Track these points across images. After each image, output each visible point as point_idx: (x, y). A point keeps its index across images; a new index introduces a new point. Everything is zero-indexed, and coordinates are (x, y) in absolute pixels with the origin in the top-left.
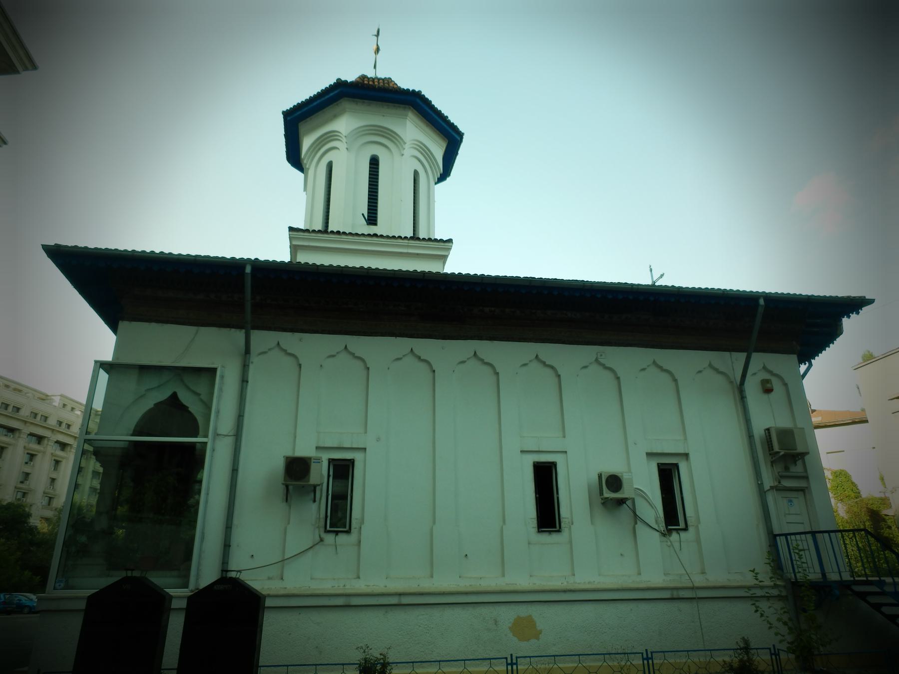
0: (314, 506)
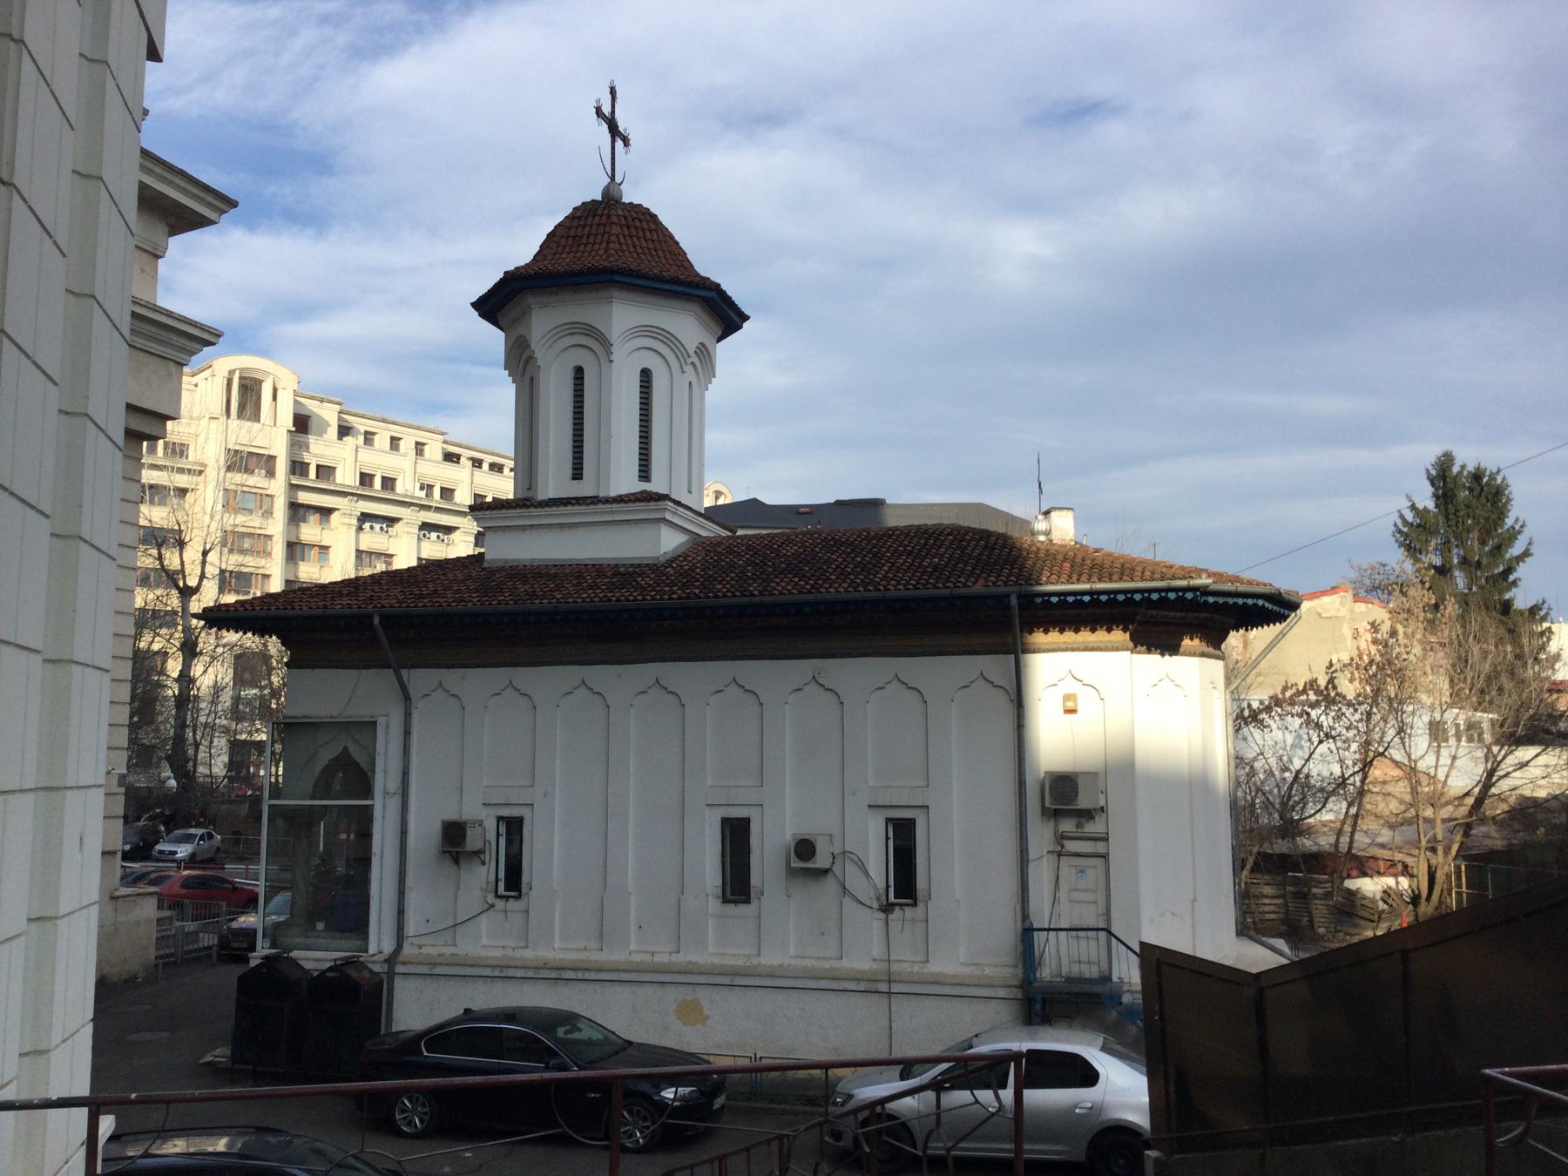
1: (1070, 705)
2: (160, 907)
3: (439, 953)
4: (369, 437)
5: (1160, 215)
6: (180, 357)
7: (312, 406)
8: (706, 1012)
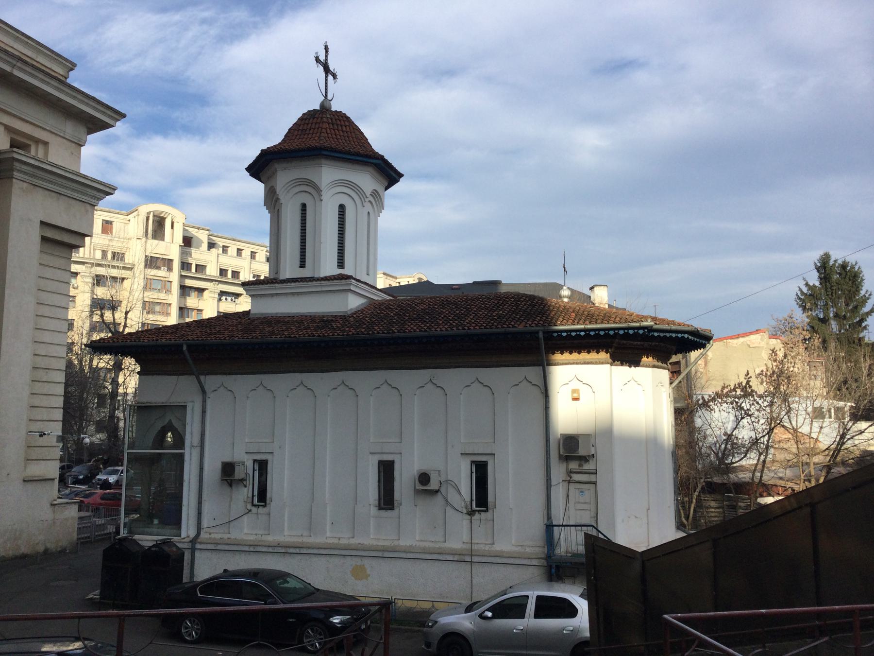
0: (246, 489)
1: (575, 395)
2: (80, 510)
3: (217, 537)
4: (225, 249)
5: (667, 123)
6: (93, 201)
7: (193, 232)
8: (368, 572)
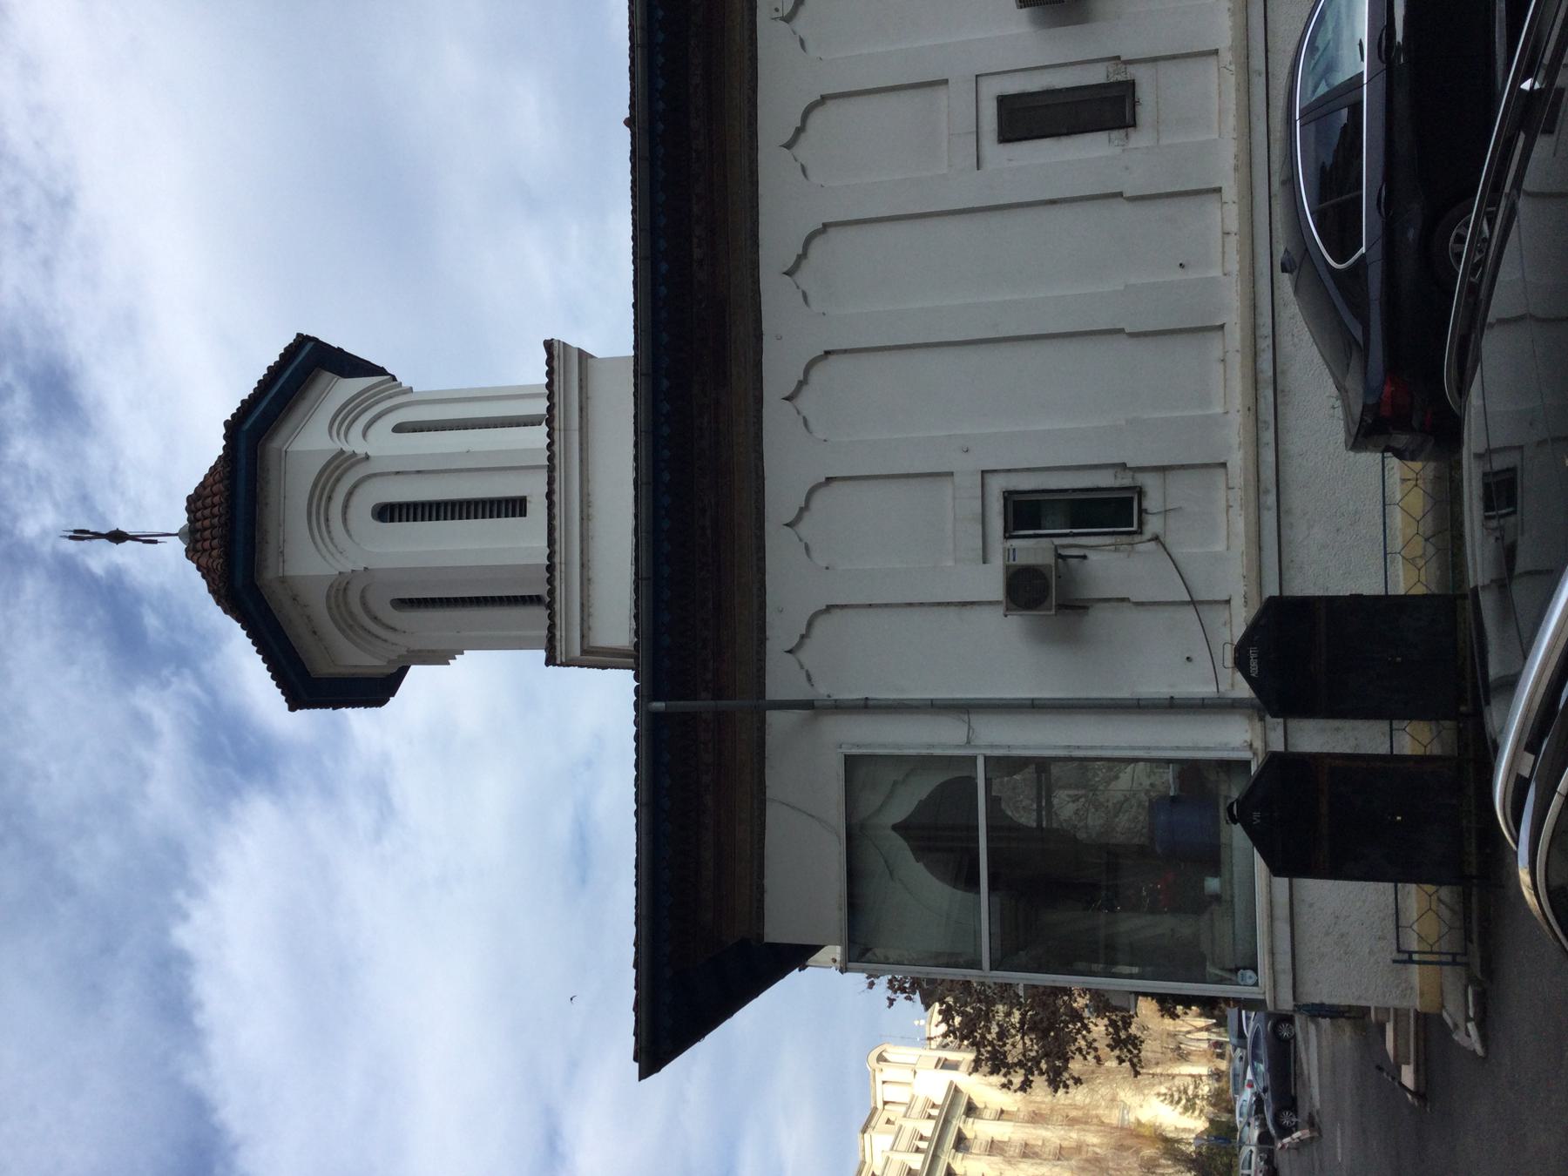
0: (1093, 556)
